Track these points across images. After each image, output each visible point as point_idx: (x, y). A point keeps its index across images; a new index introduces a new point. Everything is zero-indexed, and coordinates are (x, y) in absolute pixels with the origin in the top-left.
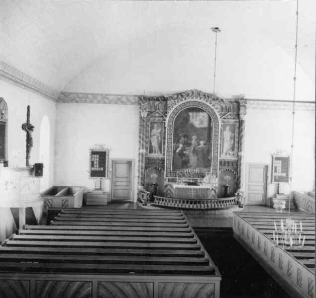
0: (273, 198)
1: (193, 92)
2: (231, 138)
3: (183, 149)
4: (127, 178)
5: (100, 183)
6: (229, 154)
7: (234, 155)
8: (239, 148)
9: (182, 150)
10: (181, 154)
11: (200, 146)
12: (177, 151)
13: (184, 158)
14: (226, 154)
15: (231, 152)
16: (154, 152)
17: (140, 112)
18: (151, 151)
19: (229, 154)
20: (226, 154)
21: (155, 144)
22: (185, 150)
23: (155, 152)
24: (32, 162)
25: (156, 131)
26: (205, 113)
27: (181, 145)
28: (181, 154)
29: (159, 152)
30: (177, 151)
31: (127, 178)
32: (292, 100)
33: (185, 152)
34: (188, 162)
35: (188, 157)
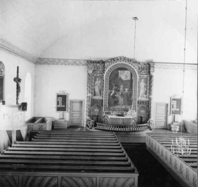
1: (121, 58)
2: (145, 86)
3: (115, 94)
4: (79, 111)
5: (62, 115)
6: (144, 97)
7: (146, 97)
9: (114, 94)
10: (114, 97)
11: (126, 92)
12: (111, 95)
13: (115, 99)
14: (142, 97)
15: (145, 96)
16: (96, 96)
17: (88, 70)
18: (95, 95)
19: (144, 97)
20: (142, 97)
21: (97, 90)
22: (116, 94)
23: (97, 96)
26: (129, 71)
27: (113, 91)
28: (114, 97)
29: (100, 96)
30: (111, 95)
31: (79, 111)
32: (183, 63)
33: (116, 96)
34: (118, 102)
35: (118, 98)
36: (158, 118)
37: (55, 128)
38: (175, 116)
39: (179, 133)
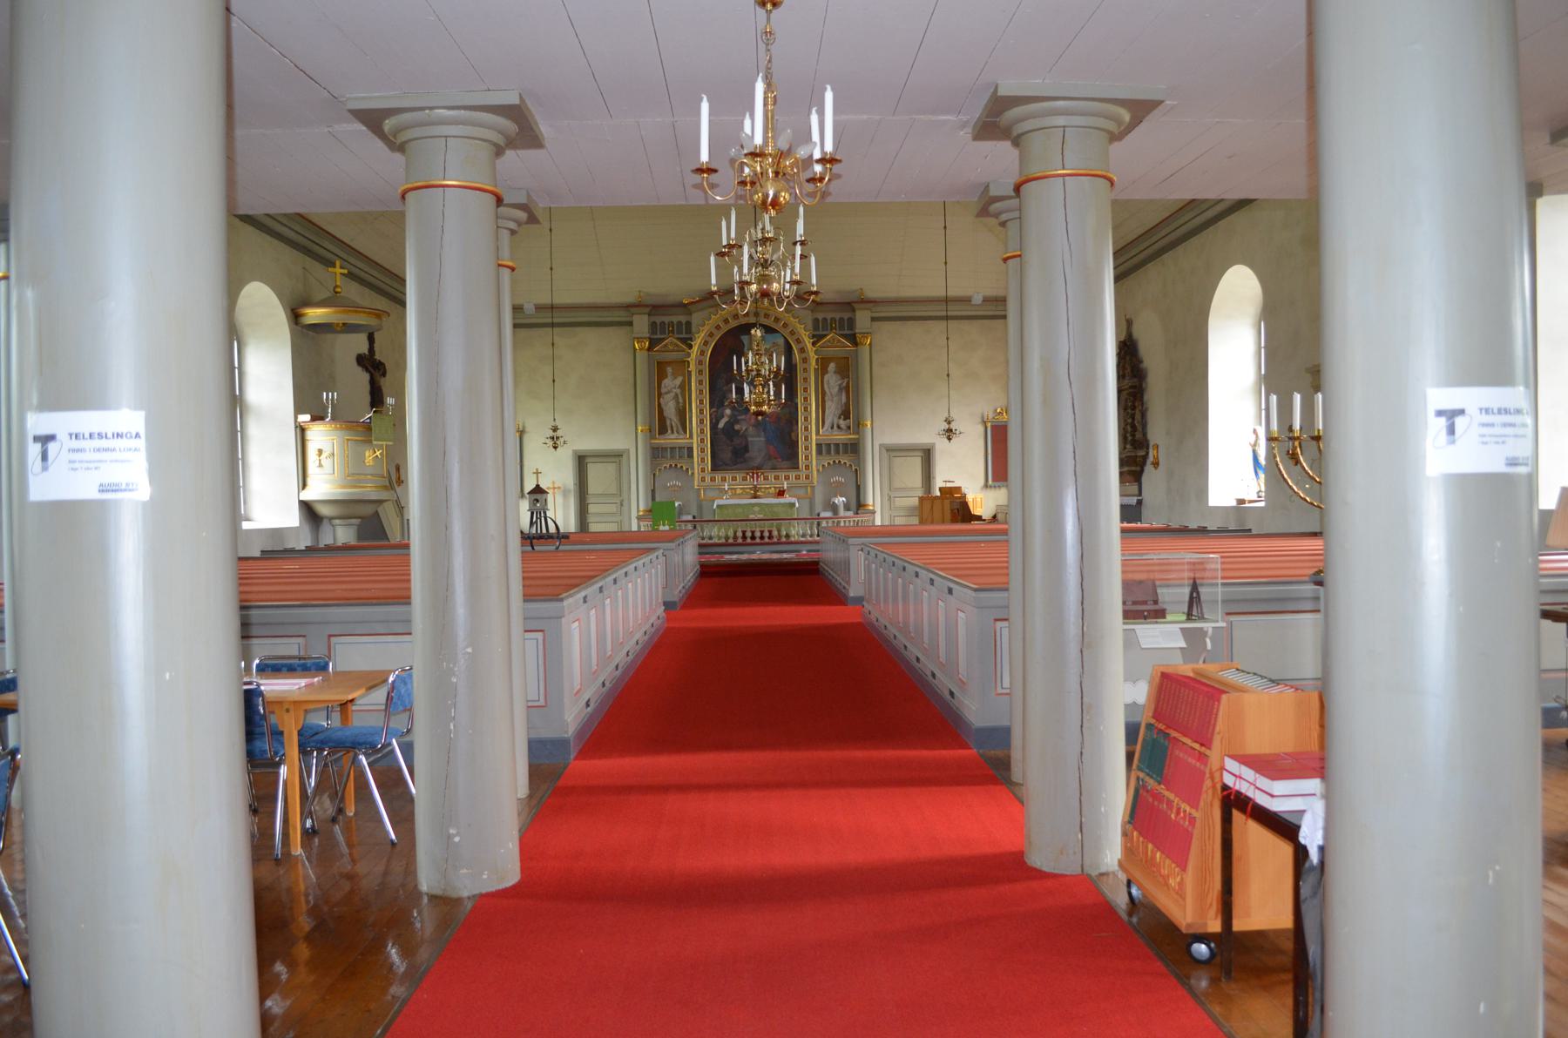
0: (783, 507)
2: (840, 389)
5: (96, 430)
8: (1314, 378)
9: (730, 424)
10: (730, 432)
12: (721, 425)
13: (737, 441)
15: (842, 423)
17: (301, 431)
18: (663, 430)
21: (670, 410)
22: (737, 422)
24: (529, 485)
25: (671, 383)
27: (728, 412)
28: (730, 432)
30: (721, 425)
32: (941, 293)
33: (737, 427)
34: (746, 449)
35: (745, 436)
36: (613, 508)
37: (593, 528)
38: (137, 435)
39: (1219, 786)
